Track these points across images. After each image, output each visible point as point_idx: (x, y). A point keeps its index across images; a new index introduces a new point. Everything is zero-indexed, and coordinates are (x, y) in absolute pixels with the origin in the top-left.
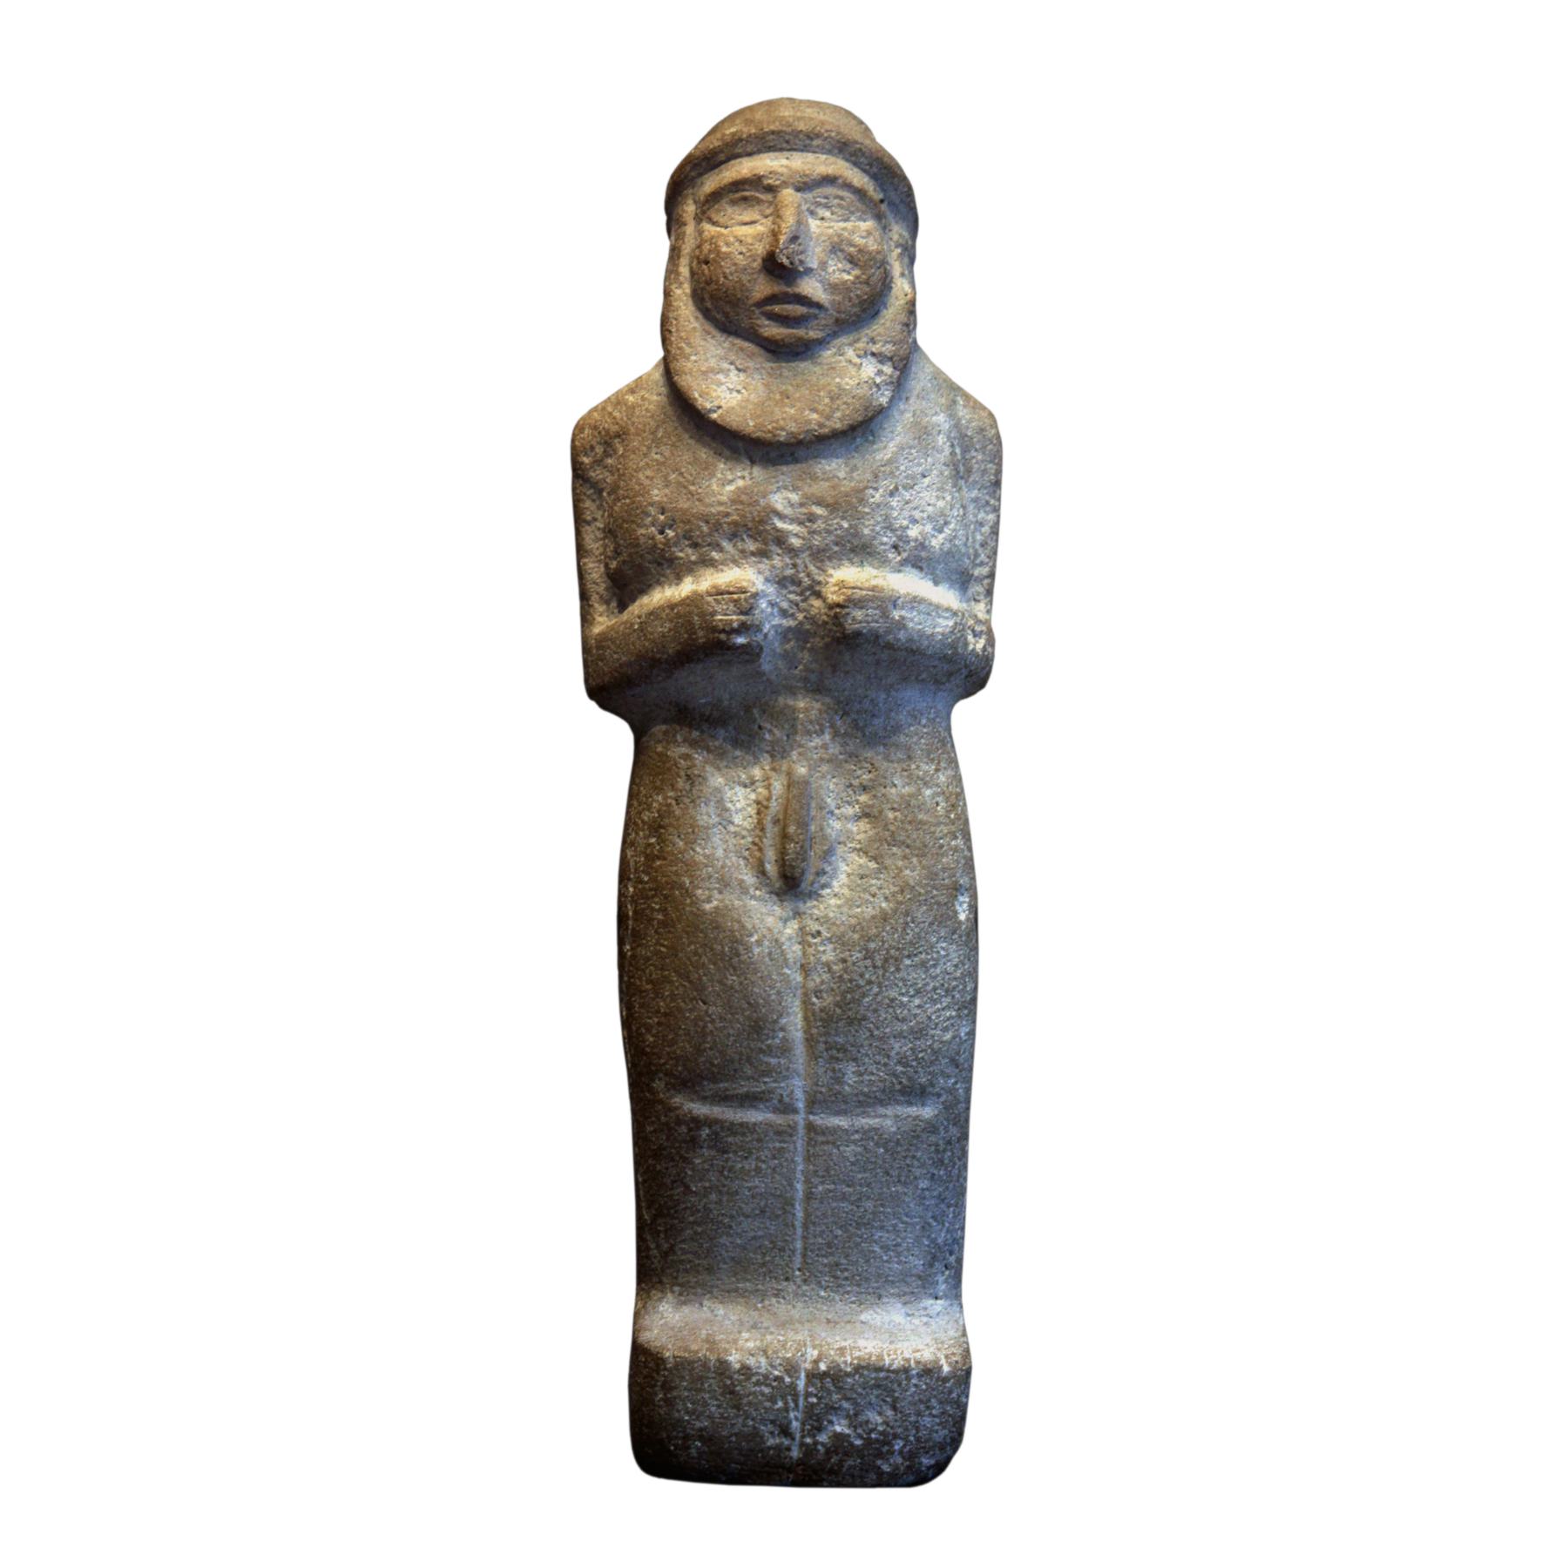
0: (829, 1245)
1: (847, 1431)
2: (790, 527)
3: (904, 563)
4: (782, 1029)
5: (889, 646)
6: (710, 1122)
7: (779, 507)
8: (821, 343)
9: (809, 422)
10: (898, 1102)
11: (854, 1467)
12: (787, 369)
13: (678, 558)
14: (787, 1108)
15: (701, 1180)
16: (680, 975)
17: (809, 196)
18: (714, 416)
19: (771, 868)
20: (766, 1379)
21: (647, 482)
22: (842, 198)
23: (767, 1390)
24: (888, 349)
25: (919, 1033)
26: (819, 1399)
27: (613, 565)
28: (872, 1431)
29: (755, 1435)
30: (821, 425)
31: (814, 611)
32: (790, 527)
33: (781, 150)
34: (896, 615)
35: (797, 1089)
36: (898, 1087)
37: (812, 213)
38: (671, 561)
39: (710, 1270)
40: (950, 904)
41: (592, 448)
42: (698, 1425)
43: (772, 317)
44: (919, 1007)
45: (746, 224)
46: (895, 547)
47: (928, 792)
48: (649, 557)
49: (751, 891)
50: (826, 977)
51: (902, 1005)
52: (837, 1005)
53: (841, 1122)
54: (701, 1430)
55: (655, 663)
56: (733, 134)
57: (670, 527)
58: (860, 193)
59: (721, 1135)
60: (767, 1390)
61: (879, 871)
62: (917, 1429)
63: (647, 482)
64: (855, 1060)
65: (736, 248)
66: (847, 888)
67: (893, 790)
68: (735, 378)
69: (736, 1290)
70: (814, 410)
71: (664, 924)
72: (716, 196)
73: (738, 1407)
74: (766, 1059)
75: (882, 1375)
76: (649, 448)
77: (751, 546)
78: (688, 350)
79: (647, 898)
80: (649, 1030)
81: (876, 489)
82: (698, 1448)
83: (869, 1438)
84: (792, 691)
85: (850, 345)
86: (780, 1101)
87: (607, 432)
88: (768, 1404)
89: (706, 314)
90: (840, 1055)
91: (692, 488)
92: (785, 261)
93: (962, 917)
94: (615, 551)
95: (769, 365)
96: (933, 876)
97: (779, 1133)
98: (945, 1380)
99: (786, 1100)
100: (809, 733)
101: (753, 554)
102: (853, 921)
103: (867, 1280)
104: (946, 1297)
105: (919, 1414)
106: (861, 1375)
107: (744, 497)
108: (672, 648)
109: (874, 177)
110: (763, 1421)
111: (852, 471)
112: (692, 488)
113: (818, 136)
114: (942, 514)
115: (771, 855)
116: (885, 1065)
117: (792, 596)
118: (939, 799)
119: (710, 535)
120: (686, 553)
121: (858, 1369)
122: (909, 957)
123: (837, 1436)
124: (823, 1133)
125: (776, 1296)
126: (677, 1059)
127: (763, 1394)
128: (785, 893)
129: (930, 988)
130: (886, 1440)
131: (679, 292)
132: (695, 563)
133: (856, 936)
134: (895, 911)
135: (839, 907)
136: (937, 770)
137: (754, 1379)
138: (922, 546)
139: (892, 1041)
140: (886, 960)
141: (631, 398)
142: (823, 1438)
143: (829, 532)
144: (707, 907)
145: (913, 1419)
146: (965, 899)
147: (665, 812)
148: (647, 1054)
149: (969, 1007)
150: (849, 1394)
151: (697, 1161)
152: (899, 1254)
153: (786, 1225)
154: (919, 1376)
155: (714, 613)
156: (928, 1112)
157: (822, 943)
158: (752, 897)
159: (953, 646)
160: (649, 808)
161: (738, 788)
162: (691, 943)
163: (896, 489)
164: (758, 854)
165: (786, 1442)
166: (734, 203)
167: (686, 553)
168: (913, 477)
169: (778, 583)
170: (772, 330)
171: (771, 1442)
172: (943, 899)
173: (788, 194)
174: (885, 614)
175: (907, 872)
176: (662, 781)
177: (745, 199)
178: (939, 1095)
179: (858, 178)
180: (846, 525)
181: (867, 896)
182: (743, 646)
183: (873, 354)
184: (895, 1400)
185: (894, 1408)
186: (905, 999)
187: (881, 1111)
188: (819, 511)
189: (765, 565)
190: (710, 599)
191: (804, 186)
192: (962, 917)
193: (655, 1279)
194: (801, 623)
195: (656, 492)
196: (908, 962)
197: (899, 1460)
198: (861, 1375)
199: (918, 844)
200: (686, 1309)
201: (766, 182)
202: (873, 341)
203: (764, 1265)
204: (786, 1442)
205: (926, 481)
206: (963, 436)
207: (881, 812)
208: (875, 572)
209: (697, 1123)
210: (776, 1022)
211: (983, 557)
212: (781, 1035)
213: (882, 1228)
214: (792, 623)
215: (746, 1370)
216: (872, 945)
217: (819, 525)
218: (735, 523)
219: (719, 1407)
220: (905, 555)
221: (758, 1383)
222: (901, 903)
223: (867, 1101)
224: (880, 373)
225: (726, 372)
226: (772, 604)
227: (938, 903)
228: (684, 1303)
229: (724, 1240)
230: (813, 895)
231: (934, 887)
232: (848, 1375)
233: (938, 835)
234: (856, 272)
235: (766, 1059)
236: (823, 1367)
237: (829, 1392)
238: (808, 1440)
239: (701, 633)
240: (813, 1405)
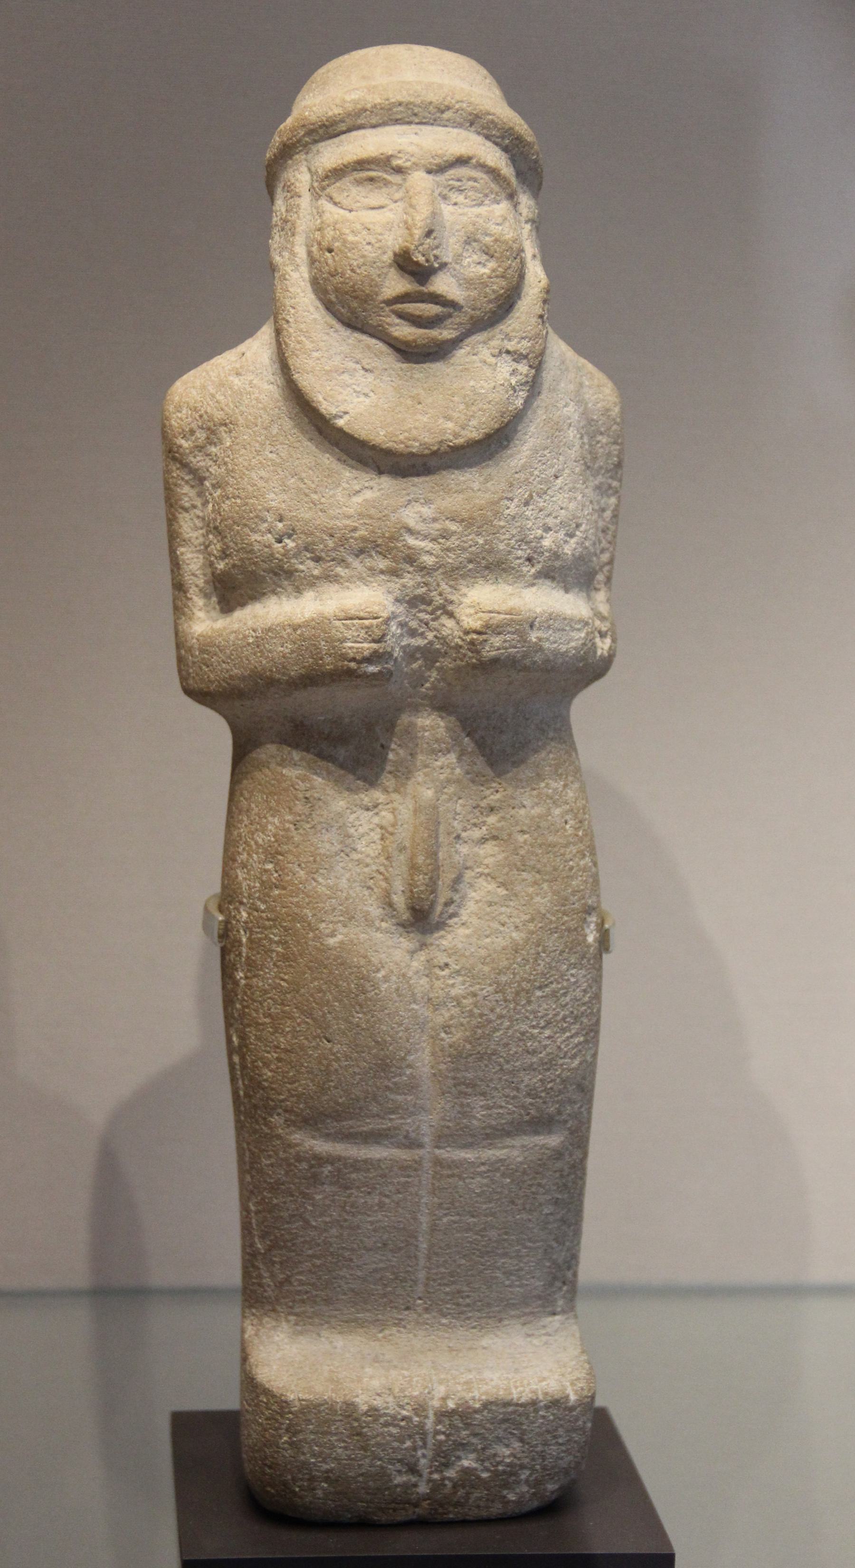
0: (451, 1275)
1: (474, 1465)
2: (422, 544)
3: (539, 575)
4: (409, 1066)
5: (526, 669)
6: (330, 1160)
7: (411, 523)
8: (456, 343)
9: (443, 431)
10: (525, 1133)
11: (480, 1499)
12: (420, 371)
13: (297, 570)
14: (413, 1144)
15: (322, 1215)
16: (303, 1012)
17: (441, 178)
18: (340, 423)
19: (399, 900)
20: (393, 1421)
21: (261, 484)
22: (475, 180)
23: (394, 1431)
24: (524, 346)
25: (549, 1064)
26: (448, 1436)
27: (221, 566)
28: (499, 1463)
29: (383, 1474)
30: (456, 435)
31: (445, 632)
32: (422, 544)
33: (410, 123)
34: (533, 636)
35: (426, 1124)
36: (527, 1118)
37: (445, 198)
38: (290, 574)
39: (328, 1301)
40: (578, 930)
41: (192, 432)
42: (325, 1467)
43: (401, 315)
44: (549, 1037)
45: (373, 208)
46: (529, 560)
47: (557, 811)
48: (265, 566)
49: (377, 923)
50: (455, 1011)
51: (533, 1037)
52: (467, 1040)
53: (468, 1155)
54: (327, 1471)
55: (271, 682)
56: (355, 102)
57: (290, 536)
58: (493, 173)
59: (343, 1172)
60: (394, 1431)
61: (507, 898)
62: (544, 1459)
63: (261, 484)
64: (483, 1094)
65: (361, 238)
66: (485, 924)
67: (522, 812)
68: (366, 381)
69: (356, 1320)
70: (448, 418)
71: (285, 958)
72: (338, 173)
73: (364, 1448)
74: (392, 1096)
75: (511, 1409)
76: (262, 445)
77: (383, 564)
78: (309, 345)
79: (265, 928)
80: (266, 1064)
81: (511, 499)
82: (323, 1489)
83: (497, 1471)
84: (416, 709)
85: (484, 343)
86: (406, 1137)
87: (211, 418)
88: (396, 1444)
89: (329, 307)
90: (469, 1090)
91: (315, 497)
92: (421, 259)
93: (590, 939)
94: (223, 551)
95: (400, 365)
96: (564, 901)
97: (403, 1168)
98: (572, 1409)
99: (413, 1135)
100: (434, 752)
101: (382, 572)
102: (483, 952)
103: (489, 1305)
104: (563, 1312)
105: (546, 1444)
106: (490, 1411)
107: (372, 511)
108: (295, 671)
109: (513, 160)
110: (391, 1461)
111: (486, 481)
112: (315, 497)
113: (448, 108)
114: (575, 517)
115: (399, 885)
116: (514, 1097)
117: (422, 615)
118: (568, 817)
119: (334, 549)
120: (307, 567)
121: (486, 1405)
122: (540, 988)
123: (466, 1471)
124: (449, 1167)
125: (395, 1325)
126: (299, 1096)
127: (391, 1435)
128: (412, 925)
129: (559, 1018)
130: (512, 1471)
131: (295, 275)
132: (317, 578)
133: (486, 969)
134: (527, 940)
135: (468, 936)
136: (565, 786)
137: (382, 1420)
138: (556, 556)
139: (522, 1074)
140: (517, 993)
141: (236, 381)
142: (451, 1473)
143: (464, 549)
144: (331, 941)
145: (539, 1449)
146: (593, 919)
147: (284, 838)
148: (264, 1089)
149: (592, 1032)
150: (477, 1430)
151: (318, 1197)
152: (520, 1278)
153: (409, 1257)
154: (547, 1407)
155: (344, 640)
156: (554, 1140)
157: (450, 976)
158: (378, 929)
159: (583, 658)
160: (264, 830)
161: (360, 812)
162: (315, 979)
163: (531, 496)
164: (384, 884)
165: (414, 1479)
166: (359, 182)
167: (307, 567)
168: (546, 481)
169: (408, 602)
170: (403, 331)
171: (398, 1480)
172: (573, 924)
173: (419, 180)
174: (523, 636)
175: (538, 899)
176: (278, 802)
177: (371, 180)
178: (566, 1122)
179: (494, 156)
180: (481, 541)
181: (495, 925)
182: (374, 674)
183: (508, 352)
184: (524, 1433)
185: (521, 1440)
186: (536, 1031)
187: (509, 1141)
188: (453, 527)
189: (395, 585)
190: (338, 623)
191: (438, 169)
192: (590, 939)
193: (268, 1307)
194: (431, 643)
195: (272, 496)
196: (539, 993)
197: (525, 1489)
198: (490, 1411)
199: (549, 869)
200: (303, 1340)
201: (395, 162)
202: (508, 337)
203: (384, 1295)
204: (414, 1479)
205: (559, 481)
206: (590, 422)
207: (510, 835)
208: (509, 589)
209: (320, 1160)
210: (403, 1059)
211: (604, 544)
212: (408, 1072)
213: (505, 1255)
214: (419, 642)
215: (374, 1412)
216: (503, 979)
217: (453, 542)
218: (364, 539)
219: (346, 1448)
220: (538, 567)
221: (386, 1424)
222: (532, 933)
223: (494, 1134)
224: (514, 372)
225: (352, 373)
226: (402, 625)
227: (569, 930)
228: (301, 1333)
229: (344, 1272)
230: (441, 925)
231: (565, 913)
232: (476, 1411)
233: (568, 857)
234: (492, 264)
235: (392, 1096)
236: (451, 1405)
237: (458, 1429)
238: (436, 1476)
239: (328, 660)
240: (441, 1442)
